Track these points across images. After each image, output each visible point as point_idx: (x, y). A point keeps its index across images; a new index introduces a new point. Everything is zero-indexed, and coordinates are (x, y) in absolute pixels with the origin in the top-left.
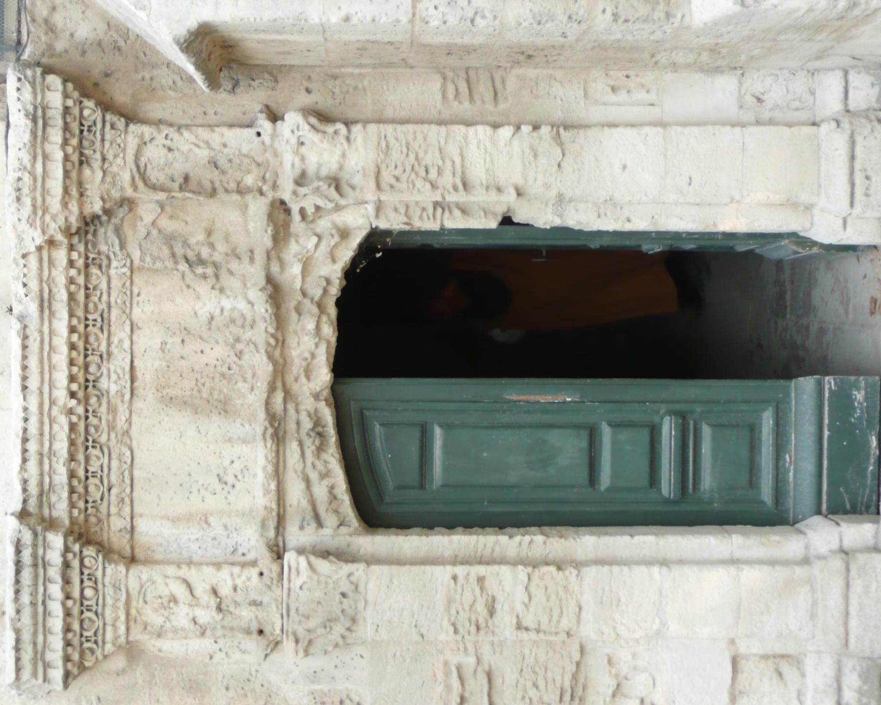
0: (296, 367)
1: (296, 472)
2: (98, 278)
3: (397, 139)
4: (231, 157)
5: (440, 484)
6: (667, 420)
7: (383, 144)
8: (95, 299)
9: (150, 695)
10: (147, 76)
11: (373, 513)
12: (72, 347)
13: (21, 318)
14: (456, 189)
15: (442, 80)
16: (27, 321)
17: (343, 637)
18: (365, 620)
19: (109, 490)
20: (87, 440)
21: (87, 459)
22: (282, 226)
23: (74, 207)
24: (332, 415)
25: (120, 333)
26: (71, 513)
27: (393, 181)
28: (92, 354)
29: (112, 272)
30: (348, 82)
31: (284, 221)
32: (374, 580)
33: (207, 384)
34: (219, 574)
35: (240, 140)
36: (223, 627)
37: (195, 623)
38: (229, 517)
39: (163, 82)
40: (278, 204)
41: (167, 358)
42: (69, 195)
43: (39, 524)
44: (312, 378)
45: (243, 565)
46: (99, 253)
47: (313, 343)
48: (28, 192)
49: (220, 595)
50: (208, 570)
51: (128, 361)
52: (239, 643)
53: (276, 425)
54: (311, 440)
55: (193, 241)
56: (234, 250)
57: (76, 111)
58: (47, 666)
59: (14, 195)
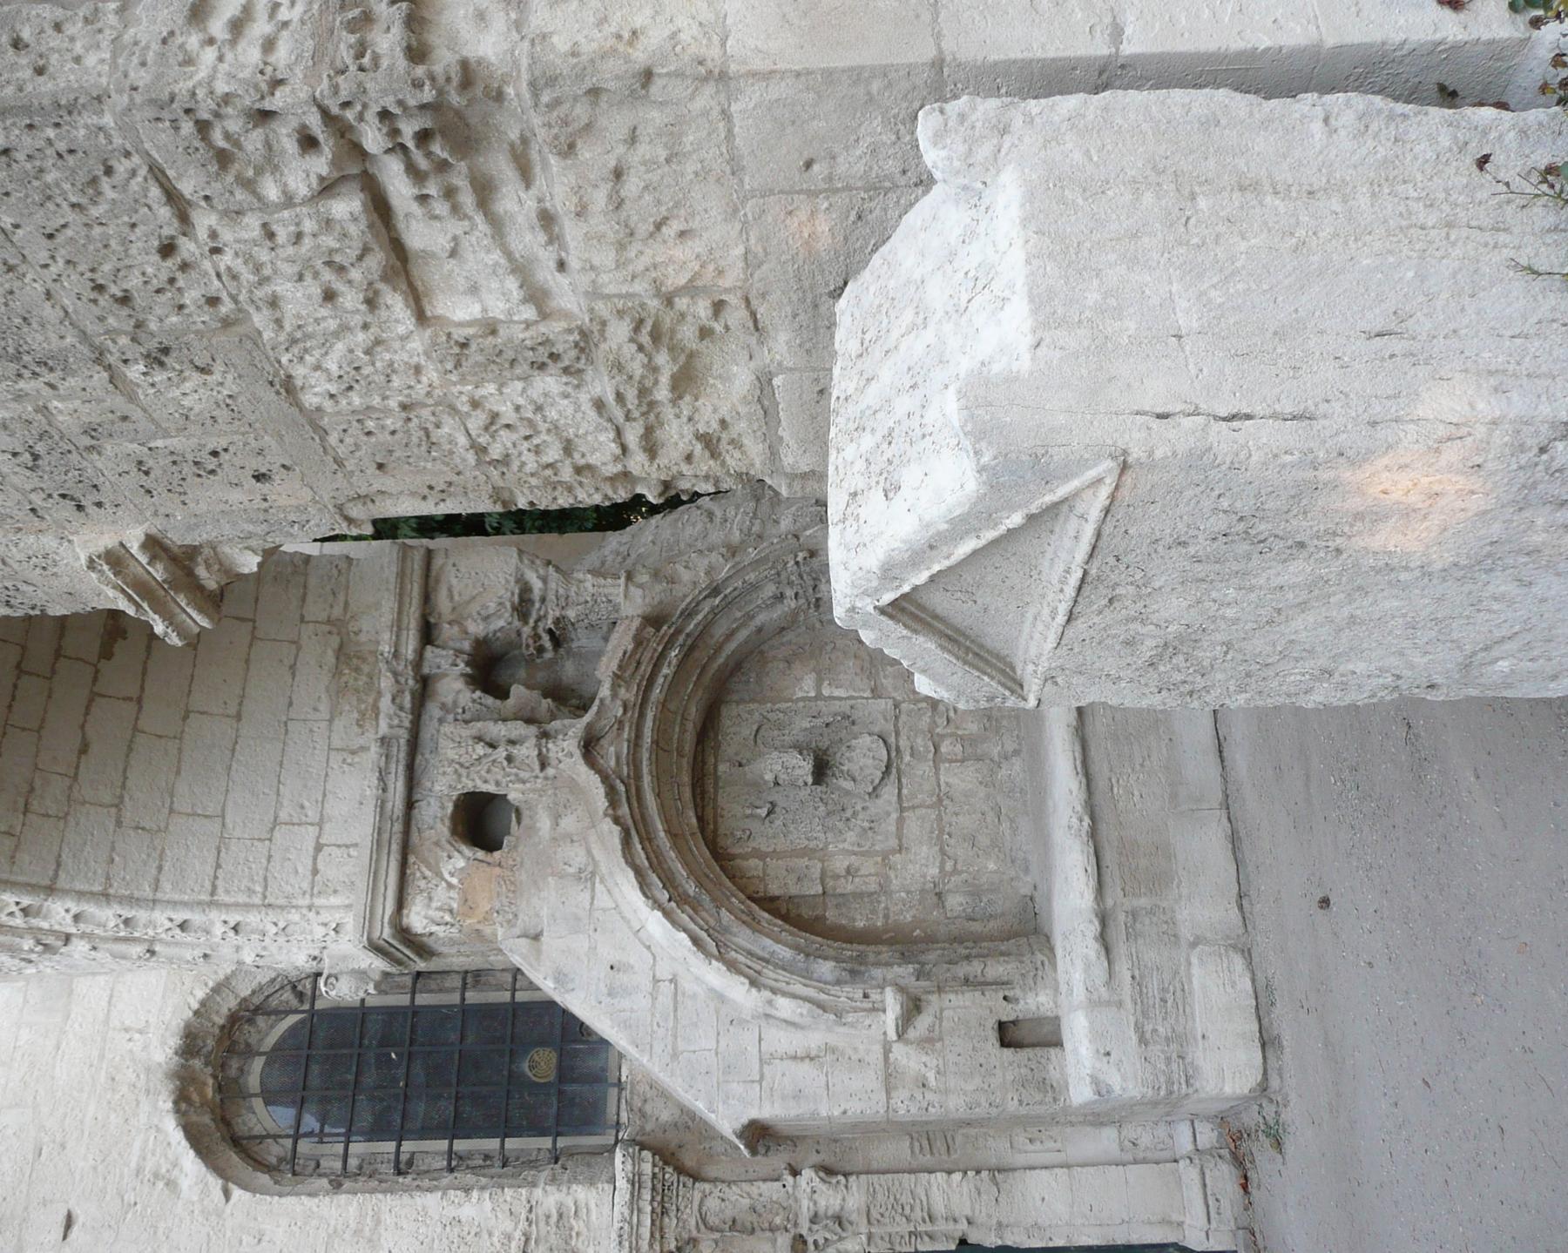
35: (770, 1191)
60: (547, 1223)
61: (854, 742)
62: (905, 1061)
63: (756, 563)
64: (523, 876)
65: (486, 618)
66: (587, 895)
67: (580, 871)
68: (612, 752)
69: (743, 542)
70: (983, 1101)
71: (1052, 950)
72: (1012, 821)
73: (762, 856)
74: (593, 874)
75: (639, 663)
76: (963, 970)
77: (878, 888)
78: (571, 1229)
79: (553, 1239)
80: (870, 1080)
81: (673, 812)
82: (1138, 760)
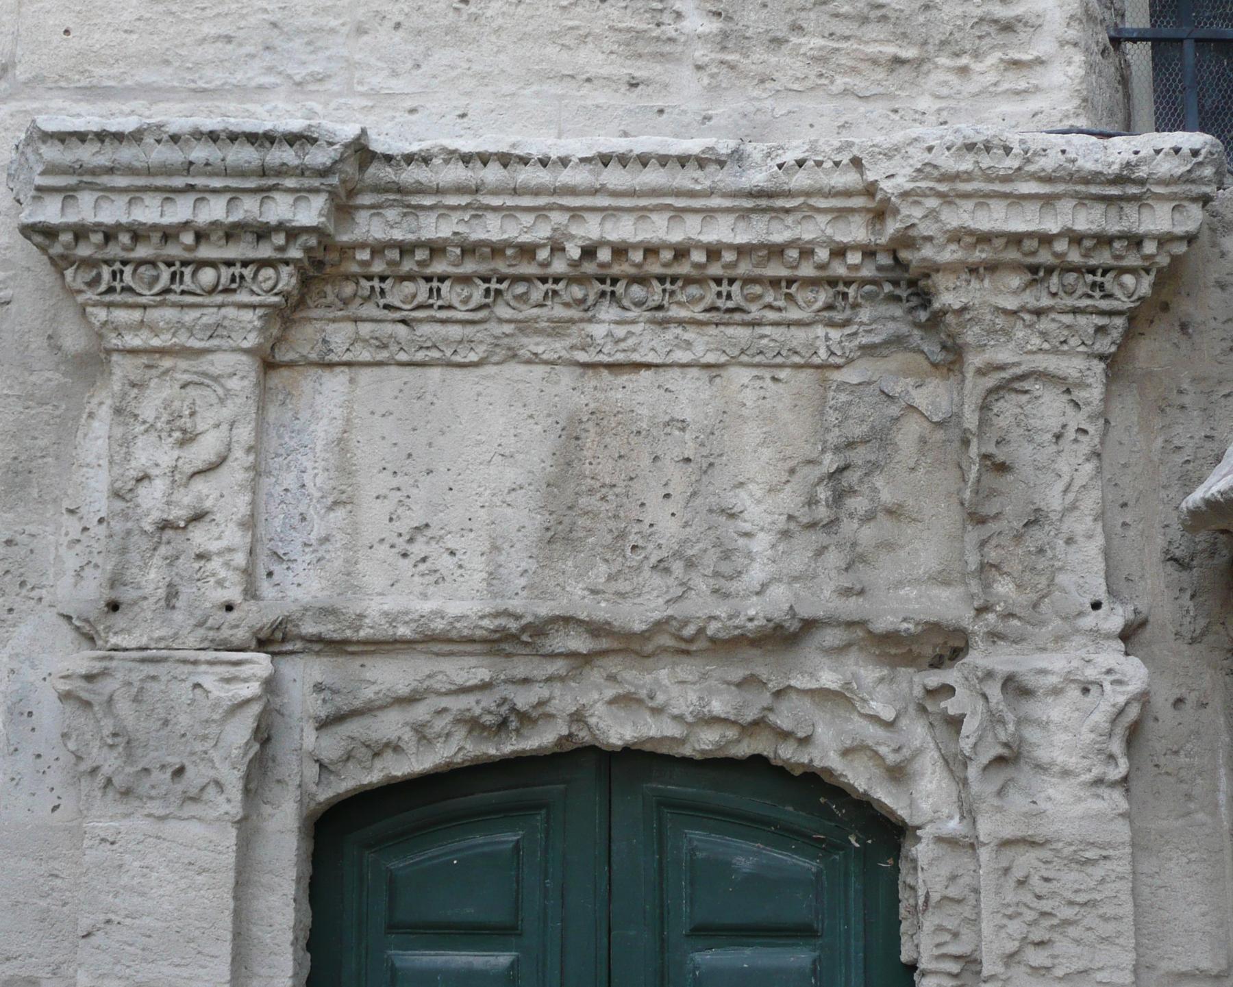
0: (635, 678)
1: (429, 676)
2: (809, 303)
3: (1102, 881)
4: (1049, 553)
5: (398, 964)
7: (1091, 854)
8: (769, 298)
9: (8, 396)
10: (1186, 400)
11: (345, 833)
12: (681, 252)
13: (737, 156)
15: (1215, 972)
17: (94, 771)
18: (127, 816)
19: (403, 321)
20: (500, 281)
21: (465, 280)
22: (911, 650)
23: (950, 254)
24: (540, 747)
25: (702, 345)
26: (363, 246)
27: (1018, 873)
28: (664, 291)
29: (820, 331)
30: (1199, 781)
31: (919, 655)
32: (207, 836)
33: (605, 506)
34: (232, 525)
35: (1082, 568)
36: (129, 533)
37: (139, 480)
38: (345, 547)
39: (1179, 429)
40: (958, 643)
41: (654, 432)
42: (974, 246)
43: (343, 182)
44: (614, 707)
45: (248, 573)
46: (855, 306)
48: (984, 166)
49: (190, 527)
50: (241, 504)
51: (651, 358)
52: (96, 566)
53: (525, 638)
54: (493, 708)
55: (879, 481)
56: (862, 559)
57: (1132, 260)
58: (68, 194)
59: (979, 139)
78: (977, 55)
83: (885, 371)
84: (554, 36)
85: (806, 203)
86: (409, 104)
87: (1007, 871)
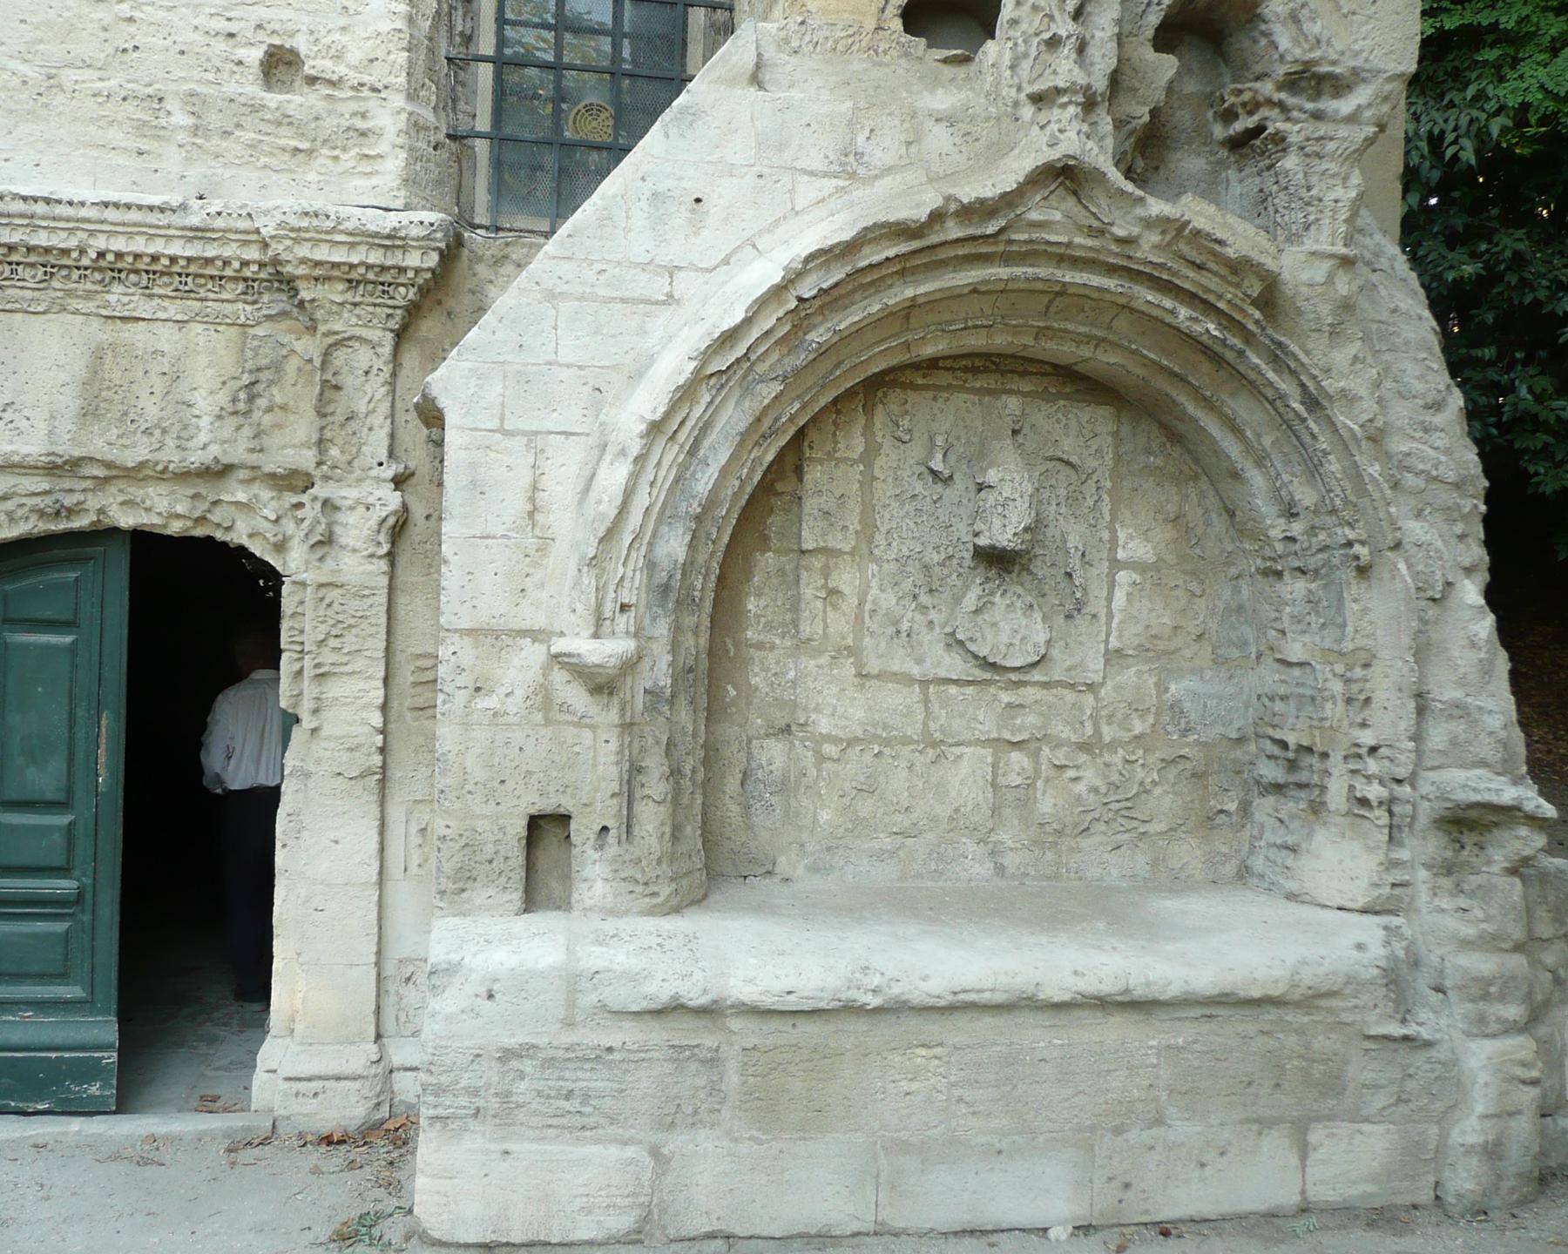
0: (136, 492)
6: (74, 884)
12: (155, 258)
13: (183, 207)
14: (317, 666)
16: (180, 213)
21: (32, 265)
25: (173, 309)
27: (327, 601)
29: (240, 305)
47: (163, 510)
55: (275, 390)
56: (263, 432)
57: (402, 280)
59: (311, 210)
60: (354, 114)
61: (1038, 616)
62: (516, 662)
63: (1356, 475)
64: (858, 64)
65: (1294, 18)
66: (818, 164)
67: (859, 155)
68: (1053, 216)
69: (1389, 456)
70: (449, 781)
71: (677, 910)
72: (893, 853)
73: (869, 456)
74: (852, 176)
75: (1200, 267)
76: (655, 764)
77: (804, 635)
78: (344, 149)
79: (330, 123)
80: (493, 605)
81: (947, 316)
82: (968, 1095)
83: (280, 330)
84: (93, 120)
85: (224, 236)
86: (5, 156)
87: (322, 599)
